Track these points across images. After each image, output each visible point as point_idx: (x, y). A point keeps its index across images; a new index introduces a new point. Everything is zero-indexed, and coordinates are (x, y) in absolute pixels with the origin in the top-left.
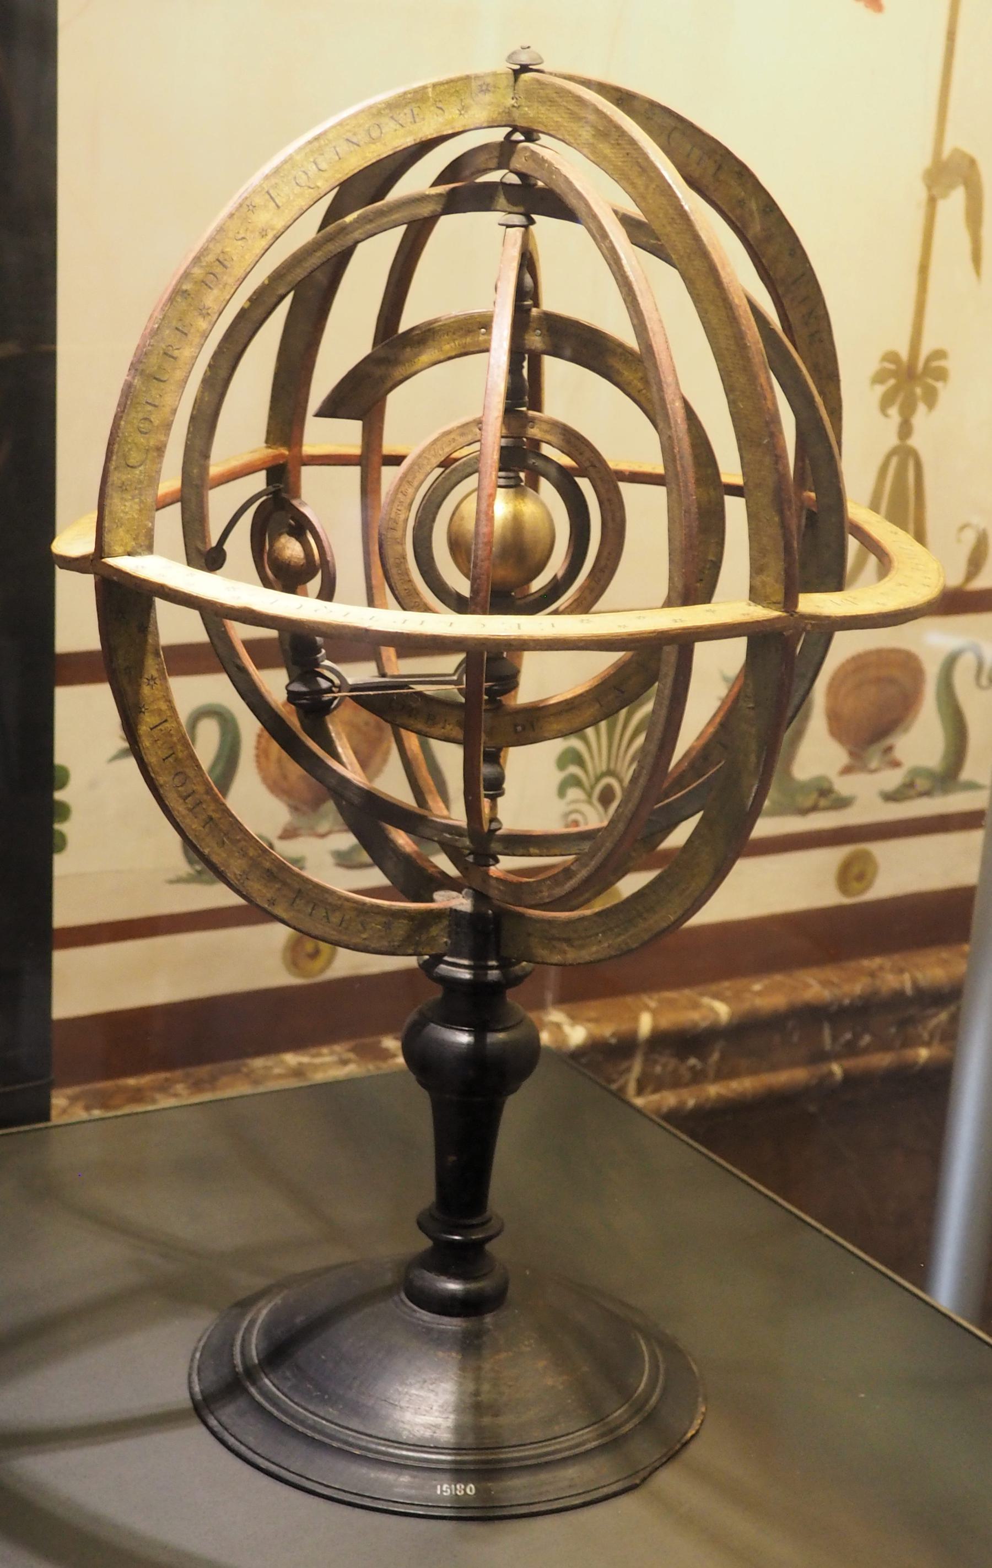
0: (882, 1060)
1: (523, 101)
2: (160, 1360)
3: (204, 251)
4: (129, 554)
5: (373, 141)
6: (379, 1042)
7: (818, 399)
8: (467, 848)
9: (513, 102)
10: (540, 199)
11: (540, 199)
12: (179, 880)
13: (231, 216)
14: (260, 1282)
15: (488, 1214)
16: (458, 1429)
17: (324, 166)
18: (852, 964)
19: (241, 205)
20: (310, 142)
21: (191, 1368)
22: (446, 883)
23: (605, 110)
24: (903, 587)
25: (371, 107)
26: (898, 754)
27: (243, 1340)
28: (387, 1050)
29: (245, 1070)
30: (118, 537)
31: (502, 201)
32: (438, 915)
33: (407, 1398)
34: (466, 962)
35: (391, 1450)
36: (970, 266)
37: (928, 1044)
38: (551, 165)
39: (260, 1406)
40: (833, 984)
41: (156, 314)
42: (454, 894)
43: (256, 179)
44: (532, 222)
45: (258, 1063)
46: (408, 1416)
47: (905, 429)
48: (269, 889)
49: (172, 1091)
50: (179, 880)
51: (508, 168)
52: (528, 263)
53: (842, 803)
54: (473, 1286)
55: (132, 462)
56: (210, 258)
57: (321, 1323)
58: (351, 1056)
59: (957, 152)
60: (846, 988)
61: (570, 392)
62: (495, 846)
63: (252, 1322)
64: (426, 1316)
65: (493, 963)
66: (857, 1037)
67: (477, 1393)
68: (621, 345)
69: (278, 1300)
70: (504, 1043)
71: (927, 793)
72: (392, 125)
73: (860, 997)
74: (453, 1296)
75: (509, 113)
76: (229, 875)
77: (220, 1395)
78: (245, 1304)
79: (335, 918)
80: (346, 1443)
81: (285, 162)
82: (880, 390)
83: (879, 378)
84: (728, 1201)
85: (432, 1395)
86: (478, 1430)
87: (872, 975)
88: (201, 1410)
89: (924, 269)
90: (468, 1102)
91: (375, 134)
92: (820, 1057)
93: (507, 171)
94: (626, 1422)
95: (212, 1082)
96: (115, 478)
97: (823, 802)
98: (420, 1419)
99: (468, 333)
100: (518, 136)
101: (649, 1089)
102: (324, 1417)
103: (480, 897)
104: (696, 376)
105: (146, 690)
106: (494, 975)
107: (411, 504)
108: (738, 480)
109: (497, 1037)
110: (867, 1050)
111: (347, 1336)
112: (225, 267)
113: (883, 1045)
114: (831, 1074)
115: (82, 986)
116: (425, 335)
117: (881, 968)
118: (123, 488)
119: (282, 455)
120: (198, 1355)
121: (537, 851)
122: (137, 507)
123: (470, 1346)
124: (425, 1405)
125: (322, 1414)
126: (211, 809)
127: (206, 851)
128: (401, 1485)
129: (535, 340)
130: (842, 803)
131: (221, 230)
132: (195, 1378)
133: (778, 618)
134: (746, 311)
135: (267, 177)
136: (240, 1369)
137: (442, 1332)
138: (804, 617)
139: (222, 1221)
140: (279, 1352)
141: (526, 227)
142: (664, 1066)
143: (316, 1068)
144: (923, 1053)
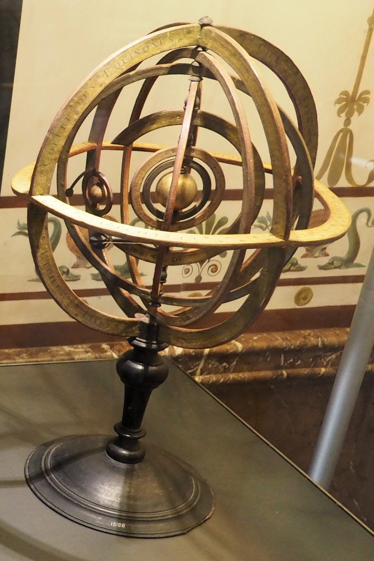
0: (306, 371)
1: (203, 37)
3: (79, 92)
4: (41, 195)
5: (145, 52)
6: (101, 345)
7: (308, 152)
8: (149, 299)
9: (199, 37)
12: (33, 280)
13: (90, 79)
15: (140, 429)
16: (121, 504)
17: (126, 61)
18: (297, 332)
19: (94, 76)
20: (122, 53)
21: (25, 466)
22: (140, 310)
23: (235, 46)
24: (333, 226)
25: (145, 40)
26: (327, 251)
27: (45, 459)
28: (104, 348)
29: (49, 351)
30: (37, 189)
31: (191, 71)
33: (104, 490)
34: (144, 341)
35: (96, 507)
37: (326, 367)
38: (211, 63)
39: (50, 485)
40: (287, 339)
41: (60, 113)
42: (143, 315)
43: (101, 66)
44: (202, 79)
45: (54, 349)
46: (103, 496)
47: (348, 122)
48: (73, 301)
49: (21, 356)
50: (33, 280)
51: (194, 59)
52: (199, 94)
53: (302, 269)
54: (132, 453)
55: (45, 164)
56: (81, 94)
58: (90, 349)
60: (293, 342)
61: (209, 141)
62: (160, 300)
63: (49, 453)
64: (113, 461)
65: (154, 342)
66: (295, 361)
67: (129, 492)
68: (231, 125)
69: (58, 446)
70: (155, 371)
71: (339, 267)
72: (153, 46)
73: (298, 346)
74: (124, 455)
75: (197, 41)
76: (63, 305)
77: (35, 477)
78: (47, 445)
79: (98, 322)
80: (80, 502)
81: (112, 60)
82: (338, 106)
83: (338, 101)
85: (113, 490)
86: (129, 505)
87: (305, 337)
88: (28, 481)
91: (146, 49)
92: (280, 367)
93: (193, 60)
94: (184, 509)
95: (37, 354)
96: (39, 169)
97: (292, 268)
98: (107, 498)
100: (200, 49)
101: (206, 373)
102: (73, 492)
105: (41, 241)
106: (154, 346)
107: (143, 178)
110: (299, 366)
111: (83, 463)
112: (86, 97)
113: (306, 365)
114: (283, 374)
117: (309, 335)
118: (41, 172)
119: (94, 146)
120: (28, 461)
121: (176, 304)
122: (45, 179)
123: (129, 474)
124: (109, 492)
125: (72, 490)
126: (59, 283)
127: (56, 297)
128: (99, 520)
129: (198, 122)
130: (302, 269)
131: (86, 84)
132: (27, 470)
133: (281, 242)
134: (282, 129)
135: (105, 66)
136: (43, 469)
137: (119, 468)
138: (291, 242)
139: (38, 411)
140: (59, 465)
141: (199, 81)
142: (213, 365)
143: (76, 353)
144: (323, 370)
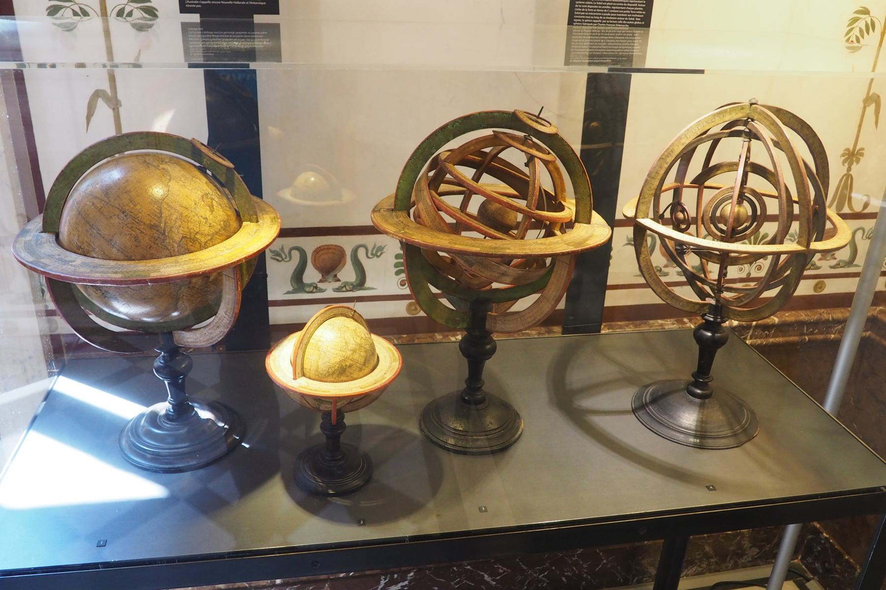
0: (821, 337)
2: (625, 398)
10: (753, 135)
11: (753, 135)
14: (651, 381)
16: (696, 426)
22: (709, 296)
26: (836, 256)
30: (640, 214)
32: (706, 304)
36: (874, 125)
43: (682, 131)
45: (651, 322)
47: (849, 169)
48: (664, 290)
52: (749, 150)
57: (664, 395)
59: (874, 94)
61: (756, 182)
71: (843, 267)
77: (638, 409)
83: (843, 155)
84: (771, 375)
86: (701, 427)
88: (634, 411)
89: (860, 126)
90: (707, 351)
92: (803, 334)
99: (733, 166)
102: (664, 418)
103: (717, 301)
104: (788, 178)
108: (797, 199)
109: (718, 335)
110: (816, 334)
113: (821, 333)
115: (612, 299)
116: (718, 168)
123: (702, 406)
124: (689, 418)
128: (681, 437)
129: (748, 169)
139: (641, 364)
140: (654, 400)
144: (833, 336)
